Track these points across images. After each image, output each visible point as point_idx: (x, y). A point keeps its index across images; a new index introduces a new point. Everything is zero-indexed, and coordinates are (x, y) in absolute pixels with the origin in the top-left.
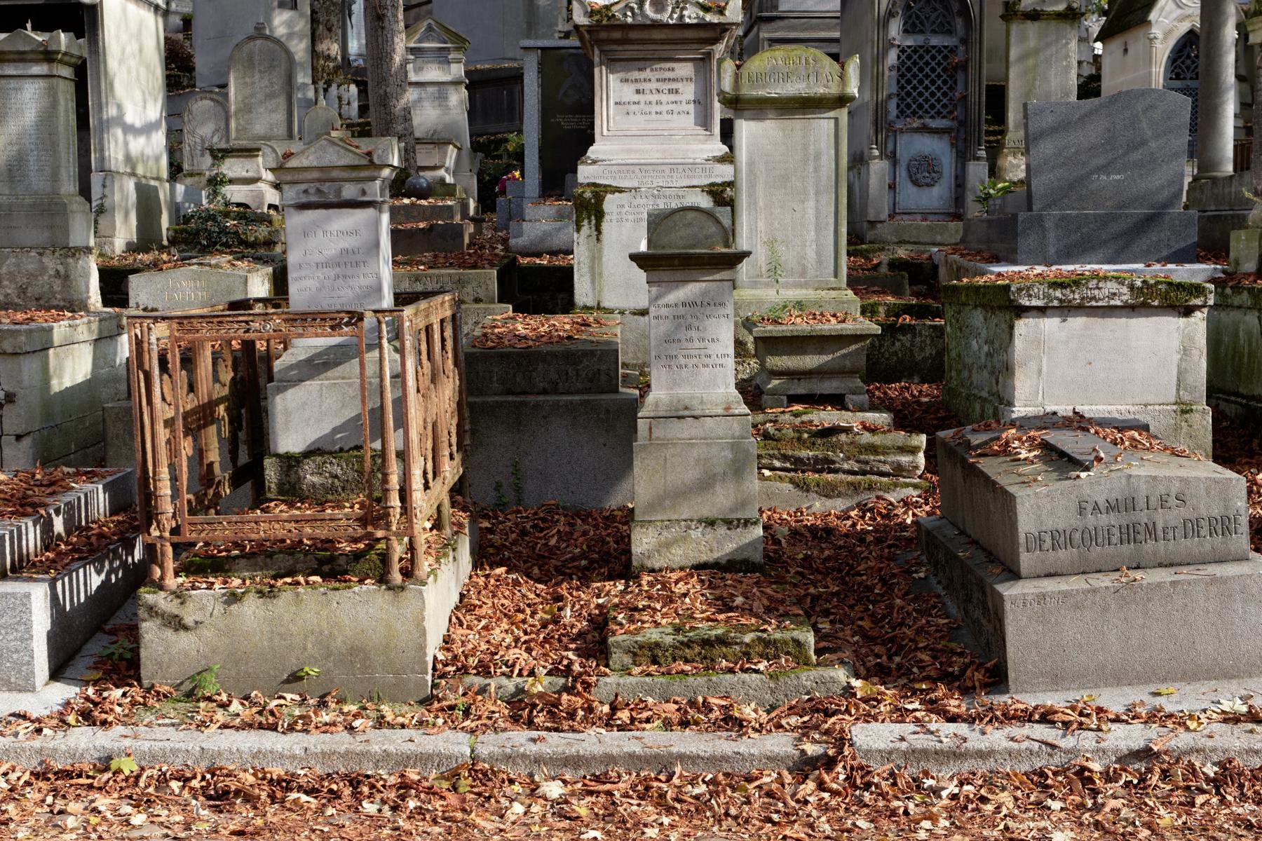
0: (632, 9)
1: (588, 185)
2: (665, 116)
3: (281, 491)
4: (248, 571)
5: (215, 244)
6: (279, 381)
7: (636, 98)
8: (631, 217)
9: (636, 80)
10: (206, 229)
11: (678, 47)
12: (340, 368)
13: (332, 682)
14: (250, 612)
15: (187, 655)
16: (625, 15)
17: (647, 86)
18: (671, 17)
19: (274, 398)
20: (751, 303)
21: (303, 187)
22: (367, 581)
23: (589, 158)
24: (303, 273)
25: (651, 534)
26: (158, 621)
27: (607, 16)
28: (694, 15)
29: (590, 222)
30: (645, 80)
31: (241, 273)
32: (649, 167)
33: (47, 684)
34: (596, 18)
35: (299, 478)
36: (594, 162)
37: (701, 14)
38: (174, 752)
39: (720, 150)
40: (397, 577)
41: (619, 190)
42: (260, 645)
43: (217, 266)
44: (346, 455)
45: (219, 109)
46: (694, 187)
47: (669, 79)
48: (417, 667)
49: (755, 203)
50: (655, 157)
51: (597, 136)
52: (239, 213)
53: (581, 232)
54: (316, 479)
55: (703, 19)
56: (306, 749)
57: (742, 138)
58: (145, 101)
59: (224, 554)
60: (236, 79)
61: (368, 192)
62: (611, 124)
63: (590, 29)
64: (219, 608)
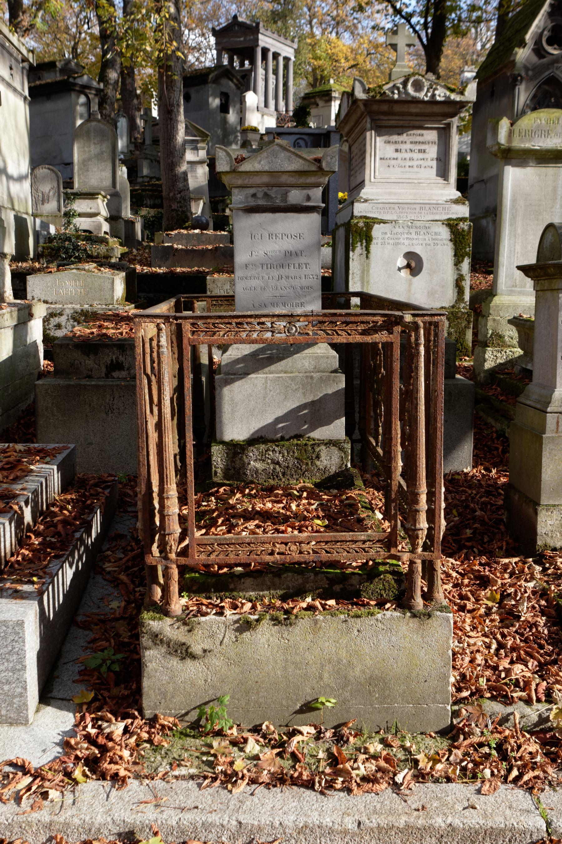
0: (398, 89)
1: (361, 217)
2: (415, 169)
3: (227, 475)
4: (254, 590)
5: (71, 257)
6: (228, 374)
7: (395, 155)
8: (391, 242)
9: (396, 142)
10: (65, 247)
11: (427, 118)
12: (283, 363)
13: (348, 712)
14: (263, 640)
15: (193, 684)
16: (393, 93)
17: (403, 147)
18: (426, 95)
19: (221, 390)
20: (509, 306)
21: (252, 191)
22: (388, 605)
23: (362, 198)
24: (249, 273)
25: (555, 517)
26: (163, 650)
27: (380, 93)
28: (442, 95)
29: (361, 245)
30: (402, 142)
32: (406, 206)
33: (37, 711)
34: (372, 94)
35: (244, 464)
36: (366, 201)
37: (448, 93)
38: (206, 826)
39: (455, 195)
40: (419, 602)
41: (384, 222)
42: (272, 674)
43: (89, 271)
44: (287, 443)
46: (436, 221)
47: (419, 142)
48: (438, 697)
49: (515, 231)
51: (367, 182)
52: (86, 236)
54: (259, 465)
55: (449, 97)
56: (359, 823)
57: (508, 180)
58: (19, 161)
59: (225, 570)
60: (78, 148)
62: (377, 174)
63: (366, 103)
64: (230, 635)
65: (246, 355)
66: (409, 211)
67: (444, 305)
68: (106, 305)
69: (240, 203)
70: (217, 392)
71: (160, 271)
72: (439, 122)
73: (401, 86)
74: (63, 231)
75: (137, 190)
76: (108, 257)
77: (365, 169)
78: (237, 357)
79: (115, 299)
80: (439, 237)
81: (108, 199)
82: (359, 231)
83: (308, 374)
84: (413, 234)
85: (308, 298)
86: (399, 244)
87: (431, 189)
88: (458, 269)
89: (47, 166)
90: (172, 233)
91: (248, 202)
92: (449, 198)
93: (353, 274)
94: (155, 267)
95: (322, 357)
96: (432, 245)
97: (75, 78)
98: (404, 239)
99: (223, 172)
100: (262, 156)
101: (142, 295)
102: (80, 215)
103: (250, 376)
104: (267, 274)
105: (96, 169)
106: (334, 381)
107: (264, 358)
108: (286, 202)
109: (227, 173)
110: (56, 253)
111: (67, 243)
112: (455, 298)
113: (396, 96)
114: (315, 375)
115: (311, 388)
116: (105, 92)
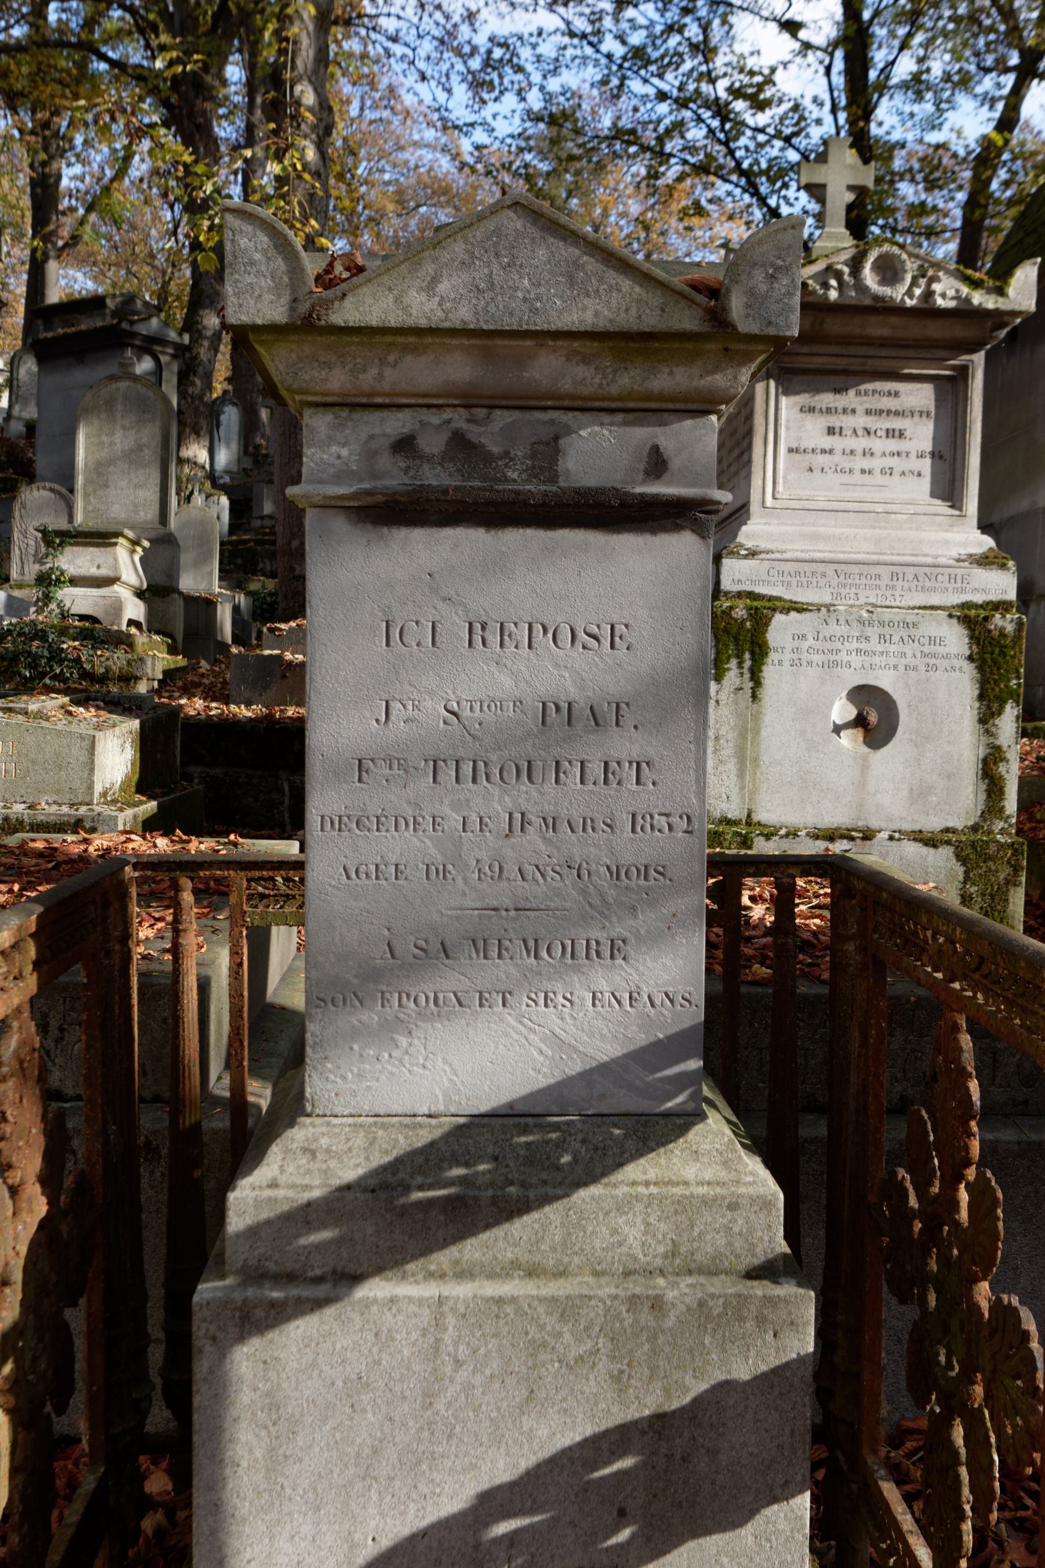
0: (838, 275)
1: (740, 595)
2: (878, 478)
5: (43, 675)
6: (255, 1275)
7: (828, 442)
8: (817, 658)
9: (829, 411)
10: (30, 653)
11: (910, 353)
12: (522, 1227)
16: (826, 286)
17: (848, 422)
18: (909, 293)
19: (222, 1356)
21: (396, 424)
23: (741, 546)
28: (951, 293)
29: (740, 665)
30: (845, 411)
31: (83, 729)
36: (753, 554)
37: (965, 290)
39: (980, 544)
41: (800, 608)
43: (40, 715)
45: (61, 504)
46: (933, 608)
47: (889, 412)
50: (861, 551)
51: (755, 507)
52: (82, 630)
53: (724, 682)
55: (968, 300)
60: (88, 436)
61: (676, 463)
62: (780, 488)
65: (348, 1187)
66: (863, 581)
67: (950, 824)
68: (72, 805)
69: (339, 478)
70: (201, 1367)
71: (244, 712)
72: (939, 361)
73: (846, 270)
74: (33, 617)
75: (246, 542)
76: (128, 678)
77: (748, 476)
78: (306, 1196)
79: (98, 788)
80: (940, 650)
81: (144, 549)
82: (734, 631)
83: (637, 1287)
84: (874, 639)
85: (646, 919)
86: (836, 663)
87: (917, 529)
88: (987, 732)
89: (47, 485)
90: (283, 626)
91: (374, 476)
92: (964, 551)
93: (717, 738)
94: (238, 704)
95: (707, 1202)
96: (922, 668)
97: (132, 323)
98: (849, 652)
99: (255, 328)
100: (445, 256)
101: (195, 770)
102: (74, 582)
103: (365, 1291)
104: (455, 806)
105: (124, 484)
106: (761, 1320)
107: (431, 1202)
108: (554, 478)
109: (273, 329)
110: (10, 666)
111: (36, 643)
112: (981, 807)
113: (833, 295)
114: (671, 1295)
115: (654, 1352)
116: (194, 352)
